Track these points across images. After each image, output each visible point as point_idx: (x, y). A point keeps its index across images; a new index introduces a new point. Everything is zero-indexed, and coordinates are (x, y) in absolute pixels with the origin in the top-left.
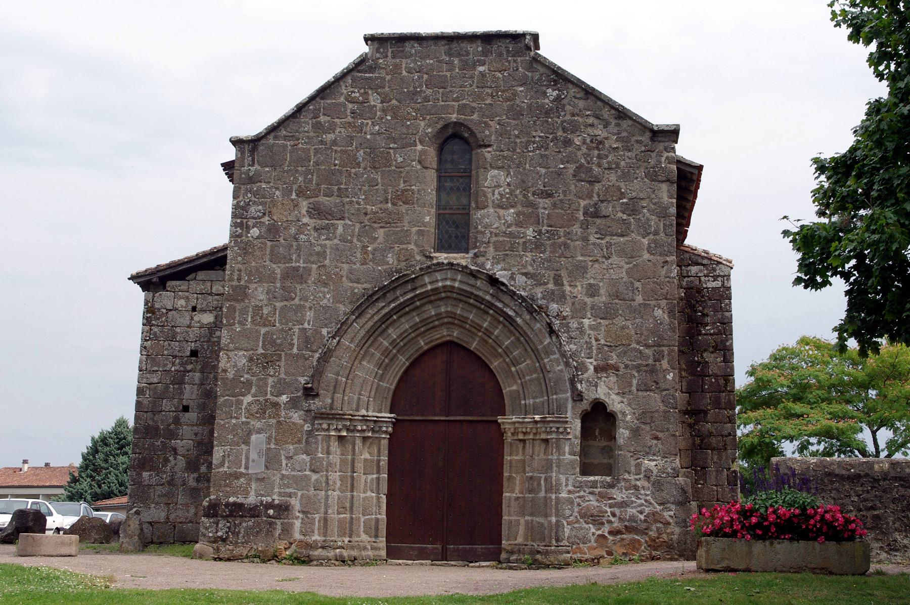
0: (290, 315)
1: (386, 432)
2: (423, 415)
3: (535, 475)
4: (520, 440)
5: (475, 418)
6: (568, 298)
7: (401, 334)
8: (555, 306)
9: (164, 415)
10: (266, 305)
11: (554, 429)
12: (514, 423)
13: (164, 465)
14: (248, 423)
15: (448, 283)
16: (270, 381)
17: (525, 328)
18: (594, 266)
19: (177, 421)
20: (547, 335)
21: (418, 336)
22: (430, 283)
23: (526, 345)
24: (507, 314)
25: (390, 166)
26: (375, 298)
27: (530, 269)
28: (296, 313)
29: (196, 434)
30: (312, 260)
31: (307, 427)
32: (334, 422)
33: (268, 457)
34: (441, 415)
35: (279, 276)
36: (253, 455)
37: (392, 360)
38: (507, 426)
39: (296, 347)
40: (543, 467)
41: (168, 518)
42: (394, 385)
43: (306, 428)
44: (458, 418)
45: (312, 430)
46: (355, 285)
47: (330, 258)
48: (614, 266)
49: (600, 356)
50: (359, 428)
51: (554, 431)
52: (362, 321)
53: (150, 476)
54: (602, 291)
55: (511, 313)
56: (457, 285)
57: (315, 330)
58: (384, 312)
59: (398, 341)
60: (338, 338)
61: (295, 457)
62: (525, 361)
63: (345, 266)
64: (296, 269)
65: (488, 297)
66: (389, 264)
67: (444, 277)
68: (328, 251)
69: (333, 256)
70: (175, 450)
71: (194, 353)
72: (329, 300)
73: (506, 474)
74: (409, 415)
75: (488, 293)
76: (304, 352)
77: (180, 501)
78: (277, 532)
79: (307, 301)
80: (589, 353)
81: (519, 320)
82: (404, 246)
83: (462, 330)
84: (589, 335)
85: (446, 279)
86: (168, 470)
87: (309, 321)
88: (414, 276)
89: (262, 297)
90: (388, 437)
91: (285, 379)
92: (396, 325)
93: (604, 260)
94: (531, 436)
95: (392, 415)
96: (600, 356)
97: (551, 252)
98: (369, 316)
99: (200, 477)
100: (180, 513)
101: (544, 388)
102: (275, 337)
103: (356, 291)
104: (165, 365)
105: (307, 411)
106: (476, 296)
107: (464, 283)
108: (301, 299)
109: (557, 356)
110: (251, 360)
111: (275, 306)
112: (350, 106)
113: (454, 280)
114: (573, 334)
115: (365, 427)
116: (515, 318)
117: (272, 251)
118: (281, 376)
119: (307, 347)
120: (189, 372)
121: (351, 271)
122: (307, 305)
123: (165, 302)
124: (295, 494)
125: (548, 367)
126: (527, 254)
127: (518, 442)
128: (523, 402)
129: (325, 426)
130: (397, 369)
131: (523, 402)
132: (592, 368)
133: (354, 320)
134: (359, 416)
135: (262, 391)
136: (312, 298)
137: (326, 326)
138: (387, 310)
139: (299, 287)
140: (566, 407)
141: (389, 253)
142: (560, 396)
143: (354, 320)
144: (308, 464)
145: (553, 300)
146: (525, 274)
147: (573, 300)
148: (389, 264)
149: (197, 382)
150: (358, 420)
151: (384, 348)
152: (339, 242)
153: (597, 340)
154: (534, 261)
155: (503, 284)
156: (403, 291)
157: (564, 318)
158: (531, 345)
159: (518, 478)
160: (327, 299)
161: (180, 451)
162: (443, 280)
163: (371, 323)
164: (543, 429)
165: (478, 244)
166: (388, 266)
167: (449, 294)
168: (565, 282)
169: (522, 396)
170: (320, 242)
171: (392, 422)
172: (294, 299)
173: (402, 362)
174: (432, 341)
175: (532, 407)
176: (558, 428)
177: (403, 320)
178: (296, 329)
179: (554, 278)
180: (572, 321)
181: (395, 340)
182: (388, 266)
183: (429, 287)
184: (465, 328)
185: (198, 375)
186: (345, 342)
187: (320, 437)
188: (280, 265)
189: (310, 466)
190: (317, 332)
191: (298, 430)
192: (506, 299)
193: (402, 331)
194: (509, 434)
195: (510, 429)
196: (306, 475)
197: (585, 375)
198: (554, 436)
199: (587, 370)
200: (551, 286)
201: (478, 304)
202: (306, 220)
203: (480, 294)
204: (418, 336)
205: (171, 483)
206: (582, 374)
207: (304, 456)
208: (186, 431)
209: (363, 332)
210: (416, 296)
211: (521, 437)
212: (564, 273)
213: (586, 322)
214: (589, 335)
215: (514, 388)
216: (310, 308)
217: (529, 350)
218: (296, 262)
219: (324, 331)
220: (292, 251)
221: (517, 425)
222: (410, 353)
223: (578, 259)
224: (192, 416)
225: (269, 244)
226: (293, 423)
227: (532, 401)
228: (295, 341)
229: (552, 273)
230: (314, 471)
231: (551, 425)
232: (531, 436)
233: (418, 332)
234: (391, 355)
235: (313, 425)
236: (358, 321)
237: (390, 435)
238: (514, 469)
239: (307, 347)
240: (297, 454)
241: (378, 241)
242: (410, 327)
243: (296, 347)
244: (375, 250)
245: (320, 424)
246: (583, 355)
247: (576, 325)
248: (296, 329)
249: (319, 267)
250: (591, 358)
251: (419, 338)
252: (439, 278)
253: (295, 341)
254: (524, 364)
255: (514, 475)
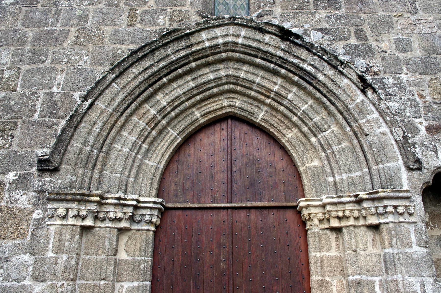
0: (37, 78)
1: (150, 222)
2: (199, 201)
3: (364, 278)
4: (333, 229)
5: (266, 204)
6: (376, 52)
7: (173, 101)
8: (362, 61)
10: (8, 69)
11: (390, 209)
12: (324, 206)
15: (230, 39)
17: (329, 84)
18: (399, 22)
20: (359, 92)
21: (193, 106)
22: (208, 40)
23: (331, 107)
24: (305, 70)
26: (140, 55)
27: (325, 25)
28: (43, 77)
30: (71, 23)
31: (37, 214)
32: (74, 205)
33: (34, 267)
34: (222, 201)
35: (30, 39)
37: (160, 133)
38: (313, 210)
39: (37, 113)
40: (375, 266)
42: (163, 164)
43: (35, 216)
44: (244, 204)
45: (43, 219)
46: (119, 46)
47: (92, 22)
48: (422, 21)
49: (430, 115)
50: (112, 215)
51: (391, 212)
52: (123, 81)
54: (415, 45)
55: (309, 69)
56: (240, 41)
57: (65, 94)
58: (151, 71)
59: (169, 109)
60: (90, 101)
61: (13, 259)
62: (329, 127)
63: (109, 29)
64: (51, 33)
65: (279, 53)
66: (160, 25)
67: (225, 33)
68: (91, 15)
69: (96, 19)
72: (86, 62)
73: (315, 278)
74: (180, 203)
75: (279, 48)
76: (47, 119)
79: (59, 63)
80: (415, 112)
81: (321, 77)
82: (178, 8)
83: (246, 99)
84: (410, 92)
85: (228, 35)
87: (59, 84)
88: (189, 31)
90: (153, 229)
91: (16, 152)
92: (167, 90)
93: (409, 15)
94: (352, 222)
95: (160, 200)
96: (430, 115)
97: (347, 9)
98: (132, 76)
101: (361, 156)
102: (13, 102)
103: (120, 52)
105: (39, 192)
106: (264, 52)
107: (249, 38)
108: (52, 62)
109: (376, 115)
111: (19, 69)
113: (237, 36)
114: (391, 91)
115: (119, 215)
116: (315, 74)
117: (26, 16)
118: (11, 148)
119: (51, 113)
121: (115, 33)
122: (59, 67)
125: (365, 130)
126: (319, 11)
127: (328, 232)
128: (331, 179)
129: (61, 212)
130: (166, 145)
131: (331, 179)
132: (423, 129)
133: (114, 80)
134: (112, 198)
136: (65, 60)
137: (79, 89)
138: (156, 68)
139: (51, 49)
140: (400, 179)
141: (160, 15)
142: (388, 165)
143: (114, 80)
144: (30, 269)
145: (358, 55)
146: (321, 30)
147: (382, 55)
148: (160, 25)
150: (111, 204)
151: (150, 117)
152: (104, 6)
153: (422, 97)
154: (328, 17)
155: (297, 36)
156: (175, 49)
157: (375, 73)
158: (338, 105)
159: (334, 283)
162: (223, 36)
163: (134, 84)
164: (373, 210)
165: (262, 5)
166: (158, 28)
167: (230, 54)
168: (369, 37)
169: (329, 171)
170: (82, 7)
171: (159, 210)
172: (44, 62)
173: (173, 137)
174: (209, 113)
175: (346, 185)
176: (396, 207)
177: (175, 85)
178: (41, 94)
179: (355, 33)
180: (386, 76)
181: (164, 108)
182: (158, 28)
183: (207, 44)
184: (248, 96)
186: (100, 105)
187: (52, 228)
188: (33, 29)
189: (33, 271)
190: (67, 96)
191: (23, 218)
192: (303, 53)
193: (173, 97)
194: (316, 222)
195: (316, 214)
196: (24, 287)
197: (417, 139)
198: (390, 218)
199: (418, 131)
200: (353, 41)
201: (266, 64)
203: (270, 49)
204: (193, 106)
206: (413, 137)
209: (123, 94)
210: (191, 54)
211: (335, 223)
212: (366, 28)
213: (404, 78)
214: (410, 92)
215: (316, 163)
216: (63, 71)
217: (336, 112)
218: (52, 26)
219: (76, 95)
220: (50, 15)
221: (329, 208)
222: (183, 126)
223: (379, 14)
225: (24, 9)
226: (19, 209)
227: (345, 176)
228: (38, 107)
229: (352, 29)
230: (37, 279)
231: (386, 202)
232: (352, 222)
233: (193, 101)
234: (160, 126)
235: (45, 210)
236: (118, 81)
237: (157, 227)
238: (326, 270)
239: (51, 113)
240: (18, 254)
241: (149, 4)
242: (184, 93)
243: (37, 113)
244: (144, 12)
245: (56, 209)
246: (408, 114)
247: (391, 81)
248: (41, 94)
249: (79, 29)
250: (420, 117)
251: (194, 109)
252: (219, 34)
254: (328, 132)
255: (327, 278)
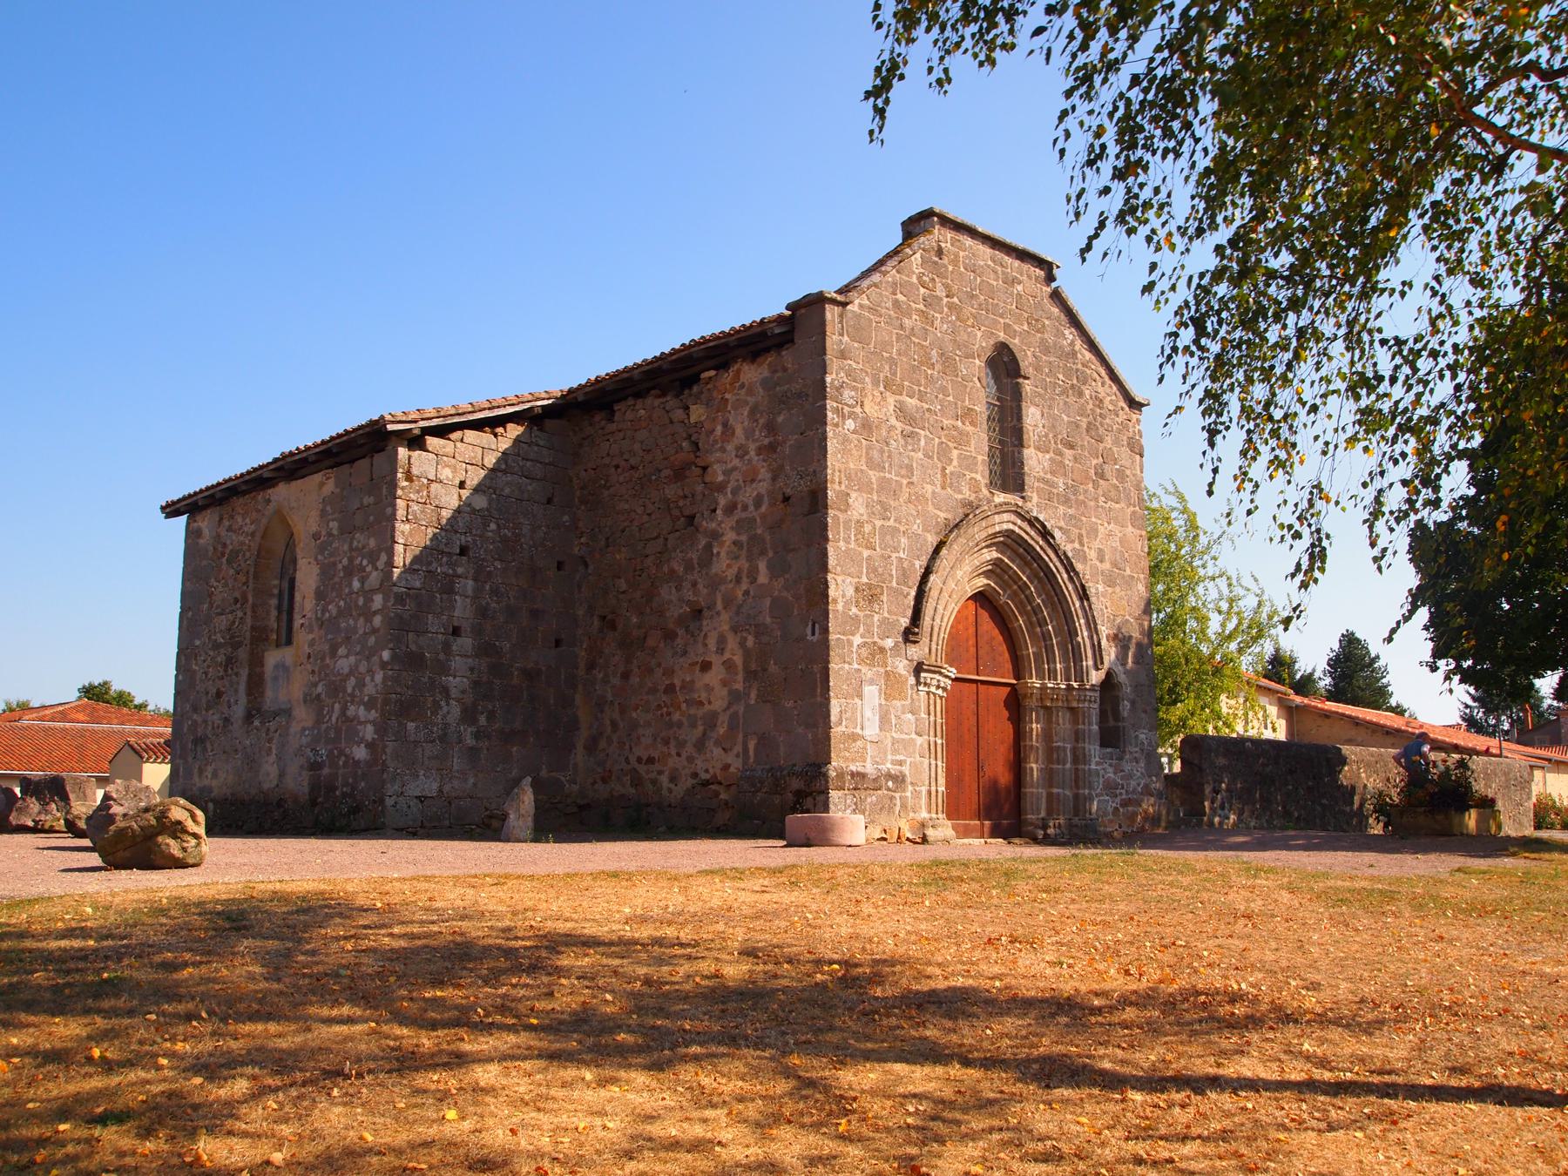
9: (432, 639)
13: (435, 713)
14: (860, 670)
16: (876, 617)
19: (447, 647)
25: (957, 376)
29: (472, 669)
36: (868, 714)
41: (441, 791)
53: (417, 727)
70: (446, 691)
71: (464, 551)
77: (455, 768)
78: (898, 808)
86: (440, 721)
89: (862, 511)
99: (478, 732)
100: (456, 783)
104: (430, 563)
110: (857, 590)
112: (922, 290)
120: (459, 577)
123: (426, 467)
124: (905, 761)
135: (869, 631)
149: (470, 592)
160: (916, 527)
161: (454, 693)
185: (471, 583)
202: (893, 421)
205: (443, 738)
207: (910, 716)
208: (457, 663)
224: (465, 642)
228: (894, 572)
253: (894, 572)
